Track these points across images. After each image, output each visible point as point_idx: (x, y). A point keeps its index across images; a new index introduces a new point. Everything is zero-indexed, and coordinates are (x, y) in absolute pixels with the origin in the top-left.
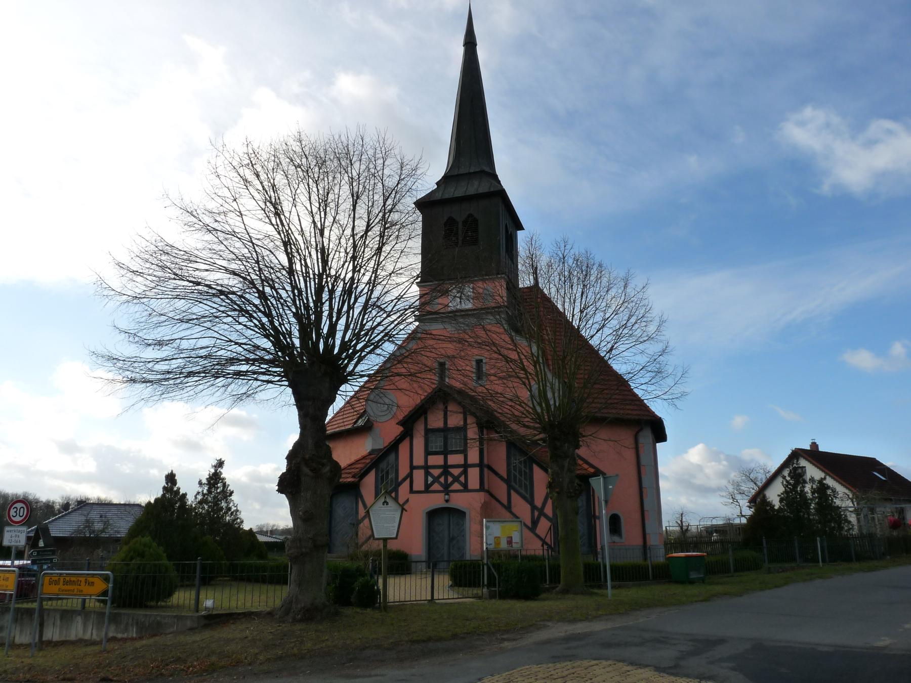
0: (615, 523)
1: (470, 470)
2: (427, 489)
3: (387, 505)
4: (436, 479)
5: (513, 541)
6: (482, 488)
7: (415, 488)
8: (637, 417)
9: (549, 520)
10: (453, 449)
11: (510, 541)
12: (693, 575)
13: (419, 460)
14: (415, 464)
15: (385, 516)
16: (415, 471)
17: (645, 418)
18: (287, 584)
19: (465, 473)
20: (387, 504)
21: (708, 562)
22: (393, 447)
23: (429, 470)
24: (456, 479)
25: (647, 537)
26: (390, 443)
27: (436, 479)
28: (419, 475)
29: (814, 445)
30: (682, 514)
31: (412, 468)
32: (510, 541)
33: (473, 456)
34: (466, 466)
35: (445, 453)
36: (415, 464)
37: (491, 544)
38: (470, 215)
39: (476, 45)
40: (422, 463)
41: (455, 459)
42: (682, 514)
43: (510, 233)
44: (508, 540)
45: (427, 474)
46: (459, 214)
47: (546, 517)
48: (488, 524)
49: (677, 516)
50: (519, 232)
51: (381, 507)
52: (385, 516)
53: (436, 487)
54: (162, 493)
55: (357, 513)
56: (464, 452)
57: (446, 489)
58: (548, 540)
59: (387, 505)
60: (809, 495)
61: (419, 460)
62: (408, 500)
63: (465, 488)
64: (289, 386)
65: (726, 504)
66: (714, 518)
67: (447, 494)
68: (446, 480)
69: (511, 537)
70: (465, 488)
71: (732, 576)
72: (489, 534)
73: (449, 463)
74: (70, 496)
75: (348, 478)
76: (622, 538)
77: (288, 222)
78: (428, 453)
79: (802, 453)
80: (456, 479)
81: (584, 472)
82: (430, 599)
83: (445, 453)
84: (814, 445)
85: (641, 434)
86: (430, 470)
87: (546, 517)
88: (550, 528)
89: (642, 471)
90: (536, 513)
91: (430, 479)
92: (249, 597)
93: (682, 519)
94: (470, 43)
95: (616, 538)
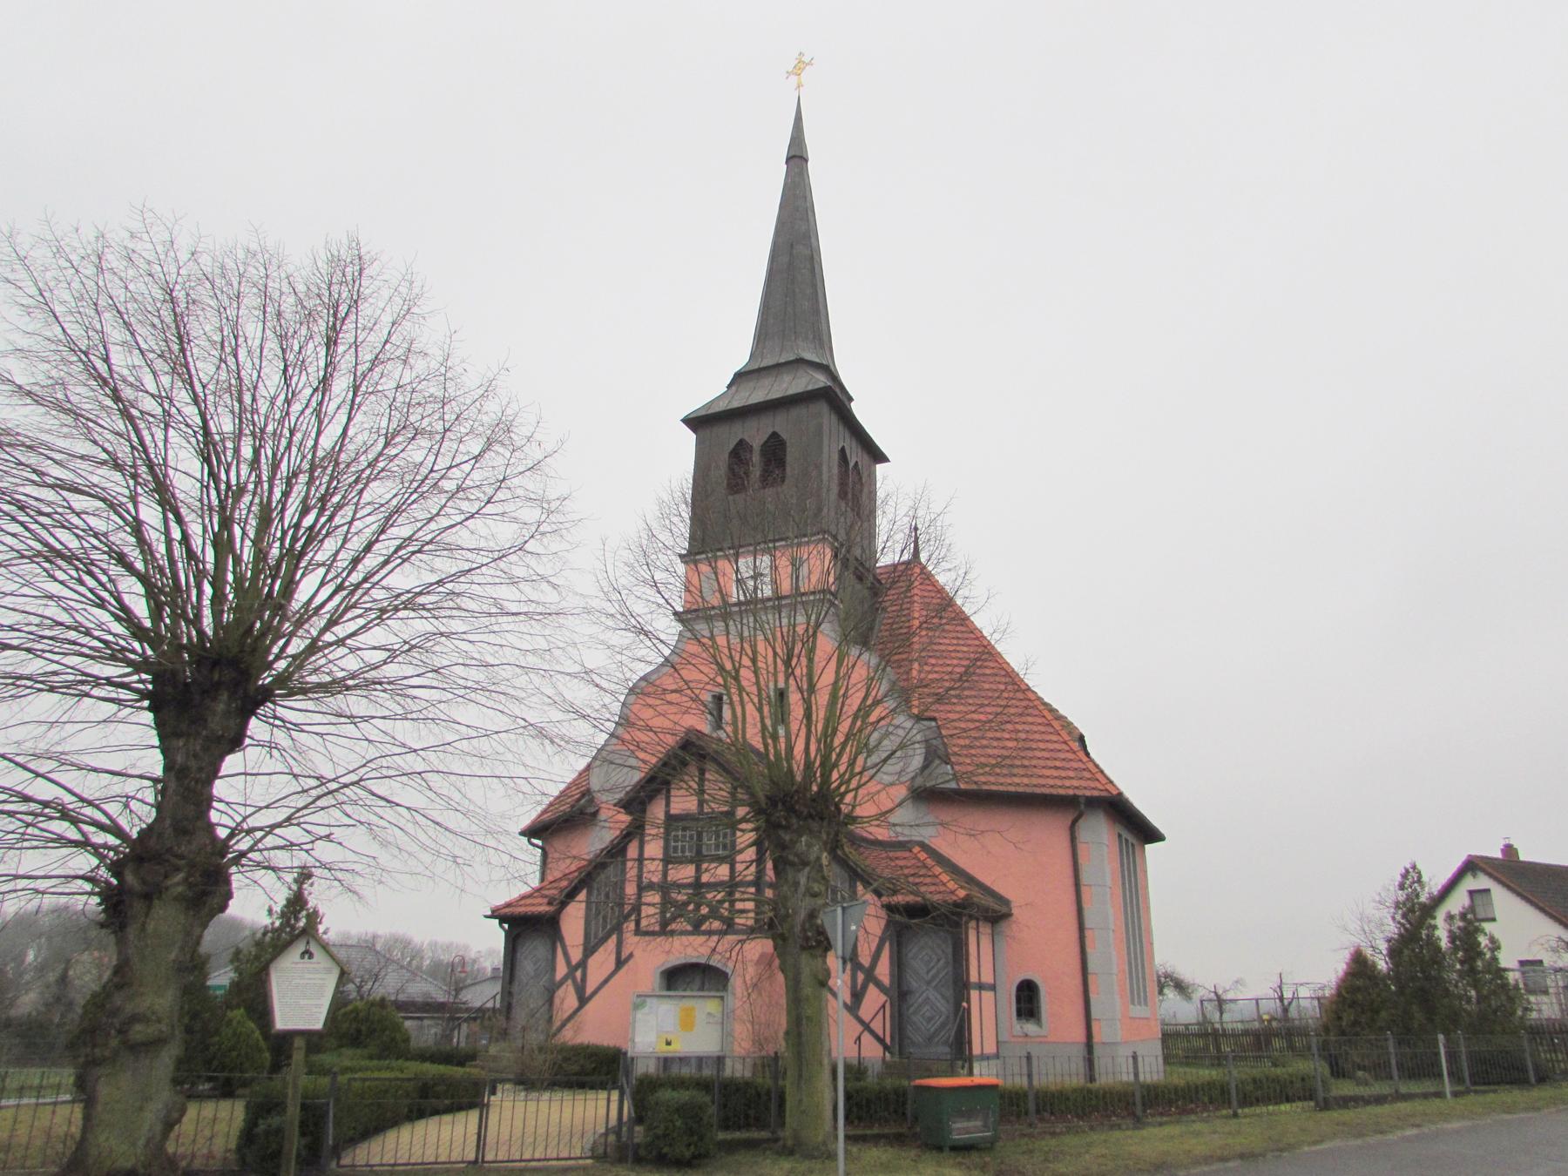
0: (1027, 999)
2: (664, 930)
3: (309, 958)
8: (1071, 792)
9: (882, 991)
15: (302, 982)
17: (1088, 793)
18: (848, 1067)
20: (311, 956)
22: (616, 851)
24: (714, 914)
26: (612, 841)
29: (1509, 850)
31: (641, 889)
34: (732, 886)
38: (774, 435)
39: (806, 161)
43: (852, 464)
46: (755, 433)
47: (879, 984)
50: (879, 467)
51: (297, 963)
52: (302, 982)
54: (503, 933)
55: (554, 969)
58: (877, 1026)
59: (309, 958)
60: (1444, 943)
61: (653, 871)
62: (631, 955)
64: (149, 709)
74: (375, 937)
76: (1041, 1027)
78: (667, 860)
79: (1481, 865)
83: (698, 859)
84: (1509, 850)
85: (1081, 821)
87: (879, 984)
88: (884, 1006)
90: (861, 977)
92: (555, 1106)
94: (797, 158)
95: (1030, 1027)
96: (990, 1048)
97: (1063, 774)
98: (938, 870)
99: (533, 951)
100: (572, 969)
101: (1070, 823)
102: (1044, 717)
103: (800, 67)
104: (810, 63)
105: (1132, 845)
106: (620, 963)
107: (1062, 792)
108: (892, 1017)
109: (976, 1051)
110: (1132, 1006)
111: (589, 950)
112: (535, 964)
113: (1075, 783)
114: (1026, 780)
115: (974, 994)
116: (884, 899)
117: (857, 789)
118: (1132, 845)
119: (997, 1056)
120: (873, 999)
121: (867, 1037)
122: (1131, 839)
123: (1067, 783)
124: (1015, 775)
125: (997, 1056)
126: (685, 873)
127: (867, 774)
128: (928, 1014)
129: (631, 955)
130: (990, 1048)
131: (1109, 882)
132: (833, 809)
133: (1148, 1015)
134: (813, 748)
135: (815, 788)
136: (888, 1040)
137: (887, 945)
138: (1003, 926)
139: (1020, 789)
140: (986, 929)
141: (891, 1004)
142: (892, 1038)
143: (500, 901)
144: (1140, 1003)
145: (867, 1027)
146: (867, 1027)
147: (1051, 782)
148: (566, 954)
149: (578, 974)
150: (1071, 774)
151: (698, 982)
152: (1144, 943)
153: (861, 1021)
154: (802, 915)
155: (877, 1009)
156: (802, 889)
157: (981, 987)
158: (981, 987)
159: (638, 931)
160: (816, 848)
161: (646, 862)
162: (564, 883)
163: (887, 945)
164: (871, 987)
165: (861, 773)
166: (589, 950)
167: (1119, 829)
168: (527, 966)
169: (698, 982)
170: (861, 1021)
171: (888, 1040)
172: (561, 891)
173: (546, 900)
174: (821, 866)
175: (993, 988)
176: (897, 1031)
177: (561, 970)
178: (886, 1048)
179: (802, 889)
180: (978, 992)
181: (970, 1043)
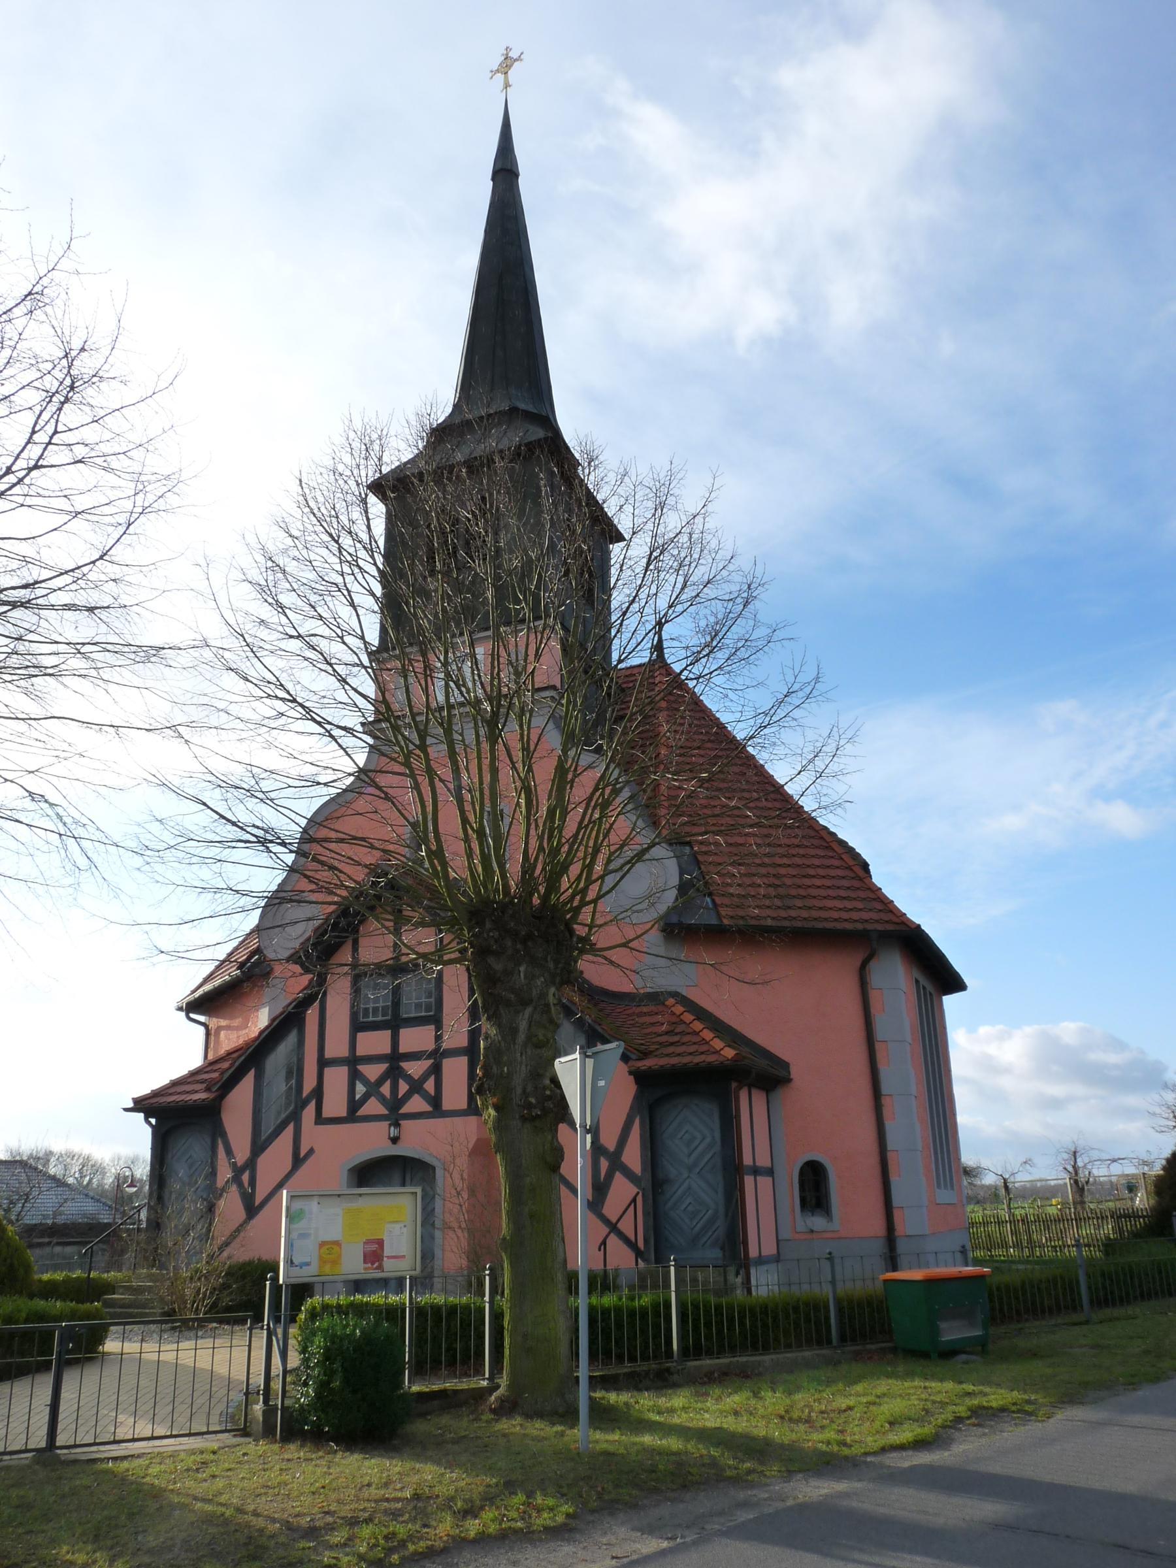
1: (448, 1064)
2: (353, 1114)
4: (373, 1089)
5: (387, 1251)
6: (472, 1110)
7: (327, 1112)
8: (859, 926)
10: (412, 1015)
11: (374, 1254)
12: (952, 1332)
13: (337, 1047)
14: (329, 1053)
16: (328, 1072)
17: (880, 927)
19: (436, 1070)
21: (1023, 1283)
23: (359, 1067)
24: (416, 1087)
25: (897, 1215)
27: (373, 1089)
28: (336, 1078)
30: (1075, 1153)
32: (374, 1254)
33: (456, 1032)
34: (438, 1056)
35: (395, 1023)
36: (329, 1053)
37: (308, 1264)
39: (517, 175)
40: (344, 1052)
41: (415, 1039)
42: (1075, 1153)
44: (374, 1247)
45: (355, 1076)
48: (298, 1205)
49: (1066, 1156)
53: (373, 1107)
54: (149, 1130)
55: (213, 1174)
56: (435, 1019)
57: (395, 1114)
58: (626, 1226)
61: (337, 1047)
62: (311, 1151)
63: (436, 1107)
65: (1163, 1129)
66: (1114, 1161)
67: (397, 1125)
68: (395, 1088)
69: (380, 1243)
70: (436, 1107)
71: (1087, 1322)
72: (303, 1236)
73: (403, 1049)
75: (196, 1092)
77: (282, 631)
78: (358, 1026)
80: (416, 1087)
81: (711, 1058)
82: (43, 1444)
86: (360, 1067)
88: (634, 1200)
89: (880, 1056)
90: (604, 1164)
91: (360, 1089)
93: (1075, 1162)
95: (818, 1222)
96: (769, 1249)
97: (849, 905)
98: (697, 1026)
99: (191, 1147)
100: (238, 1171)
101: (859, 964)
102: (822, 838)
103: (507, 63)
104: (519, 59)
105: (931, 994)
106: (298, 1161)
107: (849, 926)
108: (645, 1214)
109: (753, 1252)
110: (938, 1190)
111: (259, 1147)
112: (190, 1168)
113: (865, 915)
114: (805, 914)
115: (749, 1180)
116: (630, 1063)
117: (595, 901)
118: (931, 994)
119: (777, 1259)
120: (622, 1191)
121: (613, 1240)
122: (930, 988)
123: (855, 915)
124: (790, 908)
125: (777, 1259)
126: (375, 1042)
127: (610, 881)
128: (690, 1208)
129: (311, 1151)
130: (769, 1249)
131: (909, 1038)
132: (562, 928)
133: (955, 1201)
134: (534, 843)
135: (536, 901)
136: (641, 1244)
137: (637, 1122)
138: (779, 1094)
139: (799, 924)
140: (759, 1098)
141: (643, 1194)
142: (646, 1241)
143: (144, 1090)
144: (946, 1187)
145: (613, 1228)
146: (613, 1228)
147: (836, 915)
148: (229, 1152)
149: (246, 1177)
150: (860, 905)
151: (397, 1177)
152: (947, 1113)
153: (606, 1221)
154: (523, 1071)
155: (628, 1202)
156: (521, 1037)
157: (756, 1171)
158: (756, 1171)
159: (320, 1120)
160: (539, 981)
161: (607, 1230)
162: (226, 1065)
163: (637, 1122)
164: (618, 1177)
165: (602, 877)
166: (259, 1147)
167: (916, 974)
168: (180, 1171)
169: (397, 1177)
170: (606, 1221)
171: (641, 1244)
172: (222, 1073)
173: (203, 1086)
174: (547, 1005)
175: (770, 1172)
176: (652, 1233)
177: (225, 1173)
178: (639, 1254)
179: (521, 1037)
180: (752, 1178)
181: (745, 1243)
